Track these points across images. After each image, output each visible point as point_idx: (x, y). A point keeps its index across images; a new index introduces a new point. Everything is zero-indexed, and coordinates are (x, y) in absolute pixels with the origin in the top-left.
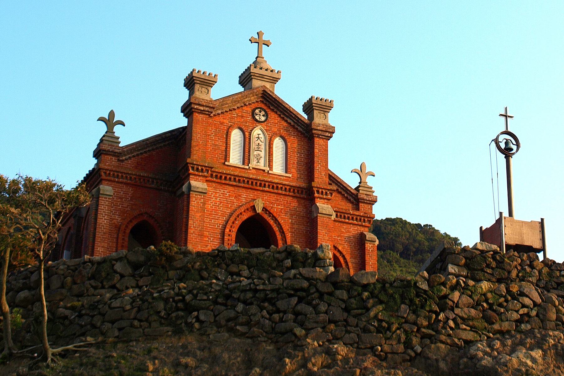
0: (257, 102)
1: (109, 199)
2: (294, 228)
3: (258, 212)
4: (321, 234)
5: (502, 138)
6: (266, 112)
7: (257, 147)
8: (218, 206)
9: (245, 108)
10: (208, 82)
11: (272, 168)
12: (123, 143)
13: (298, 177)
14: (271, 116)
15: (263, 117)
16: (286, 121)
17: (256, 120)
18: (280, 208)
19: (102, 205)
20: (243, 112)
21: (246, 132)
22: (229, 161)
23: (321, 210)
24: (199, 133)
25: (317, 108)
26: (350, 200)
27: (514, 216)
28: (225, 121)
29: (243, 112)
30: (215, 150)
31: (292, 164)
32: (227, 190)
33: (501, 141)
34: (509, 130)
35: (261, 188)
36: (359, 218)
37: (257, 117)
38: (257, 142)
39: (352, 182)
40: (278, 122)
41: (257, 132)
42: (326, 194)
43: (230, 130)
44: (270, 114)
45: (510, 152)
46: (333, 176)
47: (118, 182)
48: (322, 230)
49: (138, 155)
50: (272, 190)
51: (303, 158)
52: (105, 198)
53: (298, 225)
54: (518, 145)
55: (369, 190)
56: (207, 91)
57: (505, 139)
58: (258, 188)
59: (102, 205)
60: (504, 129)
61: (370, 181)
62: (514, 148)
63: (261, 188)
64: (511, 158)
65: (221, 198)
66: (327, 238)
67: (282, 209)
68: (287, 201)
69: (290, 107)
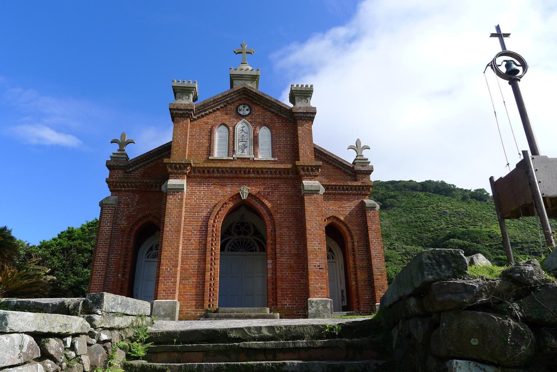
0: (240, 99)
1: (112, 207)
2: (283, 209)
3: (243, 199)
4: (309, 211)
5: (499, 60)
6: (249, 106)
7: (242, 138)
8: (201, 199)
9: (229, 107)
10: (188, 89)
11: (257, 155)
12: (131, 157)
13: (285, 160)
14: (254, 109)
15: (247, 111)
16: (270, 111)
17: (240, 115)
18: (267, 191)
19: (105, 213)
20: (227, 110)
21: (230, 126)
22: (213, 155)
23: (306, 187)
24: (179, 135)
25: (297, 94)
26: (347, 173)
27: (540, 153)
28: (209, 121)
29: (227, 110)
30: (199, 147)
31: (278, 148)
32: (211, 182)
33: (500, 64)
34: (509, 48)
35: (247, 176)
36: (357, 188)
37: (241, 113)
38: (242, 134)
39: (349, 157)
40: (262, 113)
41: (239, 126)
42: (311, 171)
43: (214, 128)
44: (253, 108)
45: (516, 76)
46: (329, 154)
47: (125, 191)
48: (309, 207)
49: (144, 165)
50: (258, 176)
51: (289, 141)
52: (109, 207)
53: (287, 204)
54: (524, 65)
55: (367, 161)
56: (187, 97)
57: (505, 61)
58: (243, 175)
59: (105, 213)
60: (500, 50)
61: (366, 154)
62: (520, 69)
63: (247, 176)
64: (518, 82)
65: (205, 191)
66: (316, 214)
67: (270, 192)
68: (275, 183)
69: (271, 98)
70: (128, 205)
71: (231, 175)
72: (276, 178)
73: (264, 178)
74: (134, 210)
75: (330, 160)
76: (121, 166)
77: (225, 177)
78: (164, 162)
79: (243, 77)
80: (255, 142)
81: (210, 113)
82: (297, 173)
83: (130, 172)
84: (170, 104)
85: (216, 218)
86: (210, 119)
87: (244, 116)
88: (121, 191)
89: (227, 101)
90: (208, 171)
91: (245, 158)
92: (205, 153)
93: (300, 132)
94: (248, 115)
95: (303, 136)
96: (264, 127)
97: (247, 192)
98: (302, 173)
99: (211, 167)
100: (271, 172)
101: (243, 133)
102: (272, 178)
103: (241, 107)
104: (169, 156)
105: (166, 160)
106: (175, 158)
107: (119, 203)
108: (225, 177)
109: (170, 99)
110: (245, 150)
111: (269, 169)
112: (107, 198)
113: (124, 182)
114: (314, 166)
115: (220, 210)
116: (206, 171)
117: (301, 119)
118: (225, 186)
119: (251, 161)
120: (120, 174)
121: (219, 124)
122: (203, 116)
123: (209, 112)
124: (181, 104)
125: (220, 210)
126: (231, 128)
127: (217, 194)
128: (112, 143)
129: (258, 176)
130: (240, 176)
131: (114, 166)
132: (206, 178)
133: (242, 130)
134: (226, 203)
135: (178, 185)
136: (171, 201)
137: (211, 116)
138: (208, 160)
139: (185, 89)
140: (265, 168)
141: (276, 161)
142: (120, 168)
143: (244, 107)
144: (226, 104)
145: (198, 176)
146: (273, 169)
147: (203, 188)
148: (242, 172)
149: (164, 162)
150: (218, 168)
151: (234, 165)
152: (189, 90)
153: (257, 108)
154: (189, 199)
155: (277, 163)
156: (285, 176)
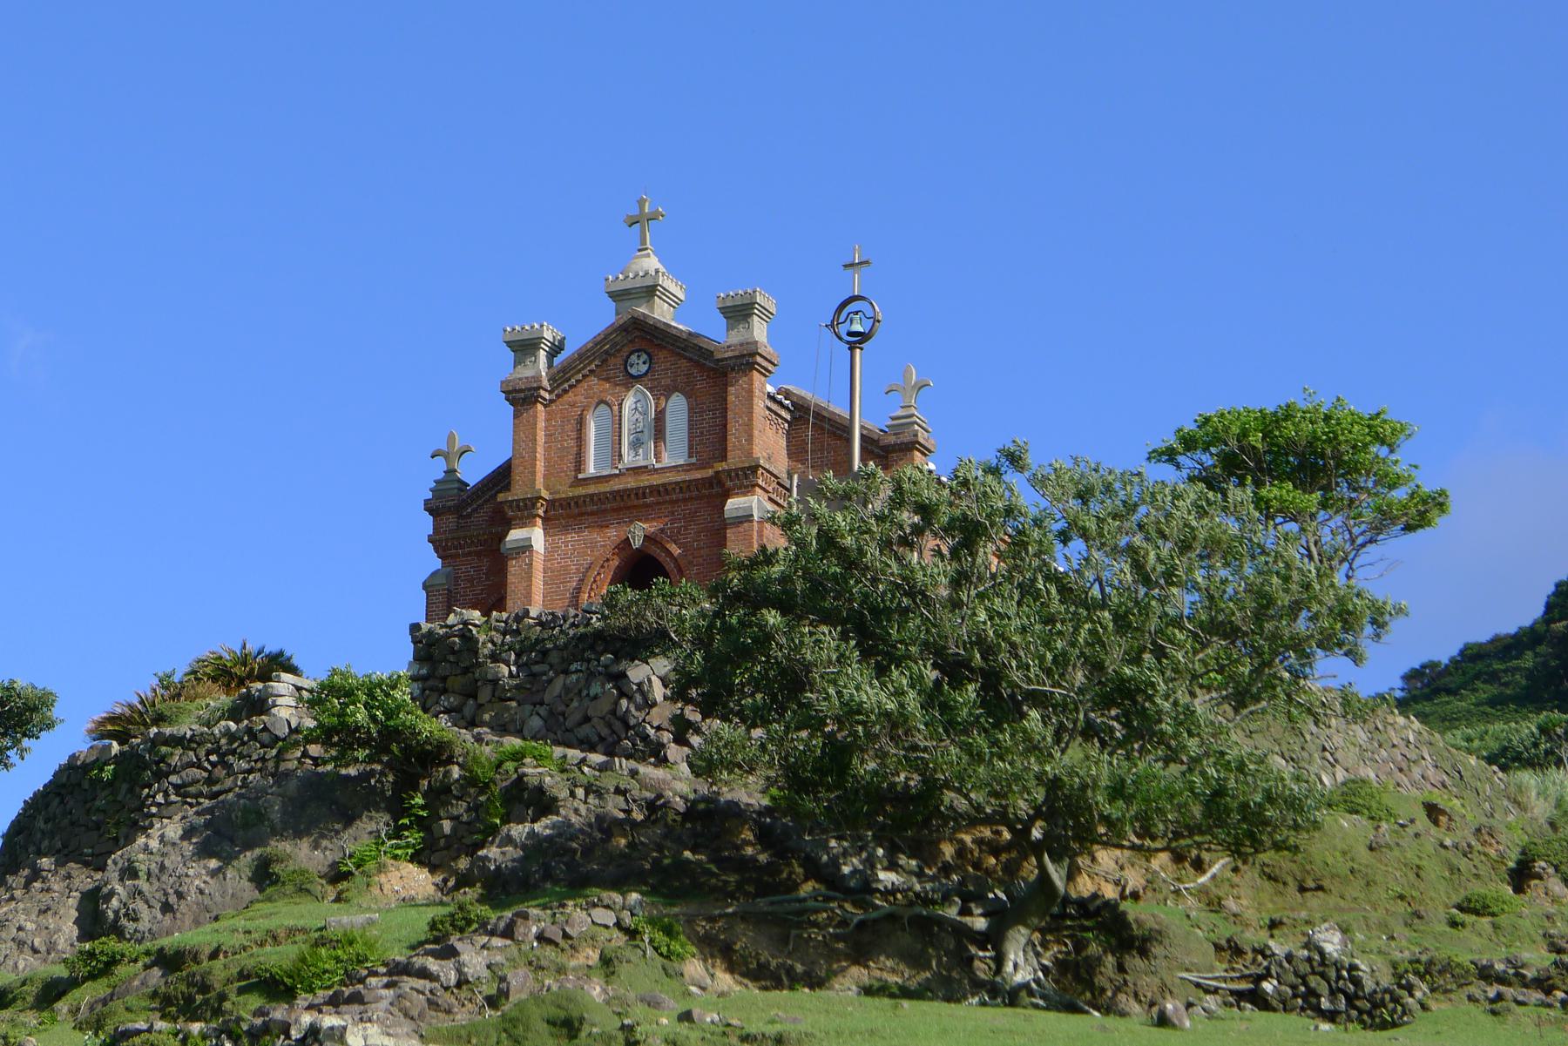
6: (648, 354)
17: (632, 376)
37: (633, 371)
38: (636, 417)
47: (465, 555)
58: (636, 502)
63: (641, 501)
70: (471, 580)
71: (615, 505)
72: (691, 498)
73: (672, 502)
74: (482, 590)
75: (837, 428)
76: (450, 507)
77: (605, 511)
78: (499, 500)
79: (630, 294)
80: (659, 432)
81: (578, 381)
82: (721, 484)
83: (469, 516)
84: (502, 382)
85: (592, 589)
86: (577, 396)
87: (638, 378)
88: (457, 555)
89: (606, 352)
90: (576, 503)
91: (640, 468)
92: (572, 466)
93: (731, 398)
94: (647, 372)
95: (736, 405)
96: (677, 393)
97: (641, 534)
98: (729, 484)
99: (579, 497)
100: (681, 488)
101: (637, 415)
102: (685, 500)
103: (634, 358)
104: (507, 488)
105: (501, 497)
106: (518, 492)
107: (457, 579)
108: (605, 511)
109: (504, 366)
110: (641, 450)
111: (677, 483)
112: (434, 574)
113: (459, 538)
114: (748, 468)
115: (599, 574)
116: (572, 504)
117: (733, 369)
118: (607, 527)
119: (650, 471)
120: (450, 521)
121: (594, 403)
122: (565, 391)
123: (577, 381)
124: (520, 379)
125: (599, 574)
126: (616, 408)
127: (593, 545)
128: (432, 457)
129: (661, 499)
130: (629, 504)
131: (438, 507)
132: (574, 517)
133: (636, 409)
134: (608, 560)
135: (522, 540)
136: (513, 567)
137: (581, 389)
138: (578, 482)
139: (527, 342)
140: (670, 484)
141: (693, 464)
142: (449, 510)
143: (639, 356)
144: (604, 356)
145: (562, 515)
146: (684, 481)
147: (572, 537)
148: (632, 496)
149: (499, 500)
150: (592, 496)
151: (616, 485)
152: (535, 344)
153: (662, 355)
154: (549, 560)
155: (697, 469)
156: (707, 492)
